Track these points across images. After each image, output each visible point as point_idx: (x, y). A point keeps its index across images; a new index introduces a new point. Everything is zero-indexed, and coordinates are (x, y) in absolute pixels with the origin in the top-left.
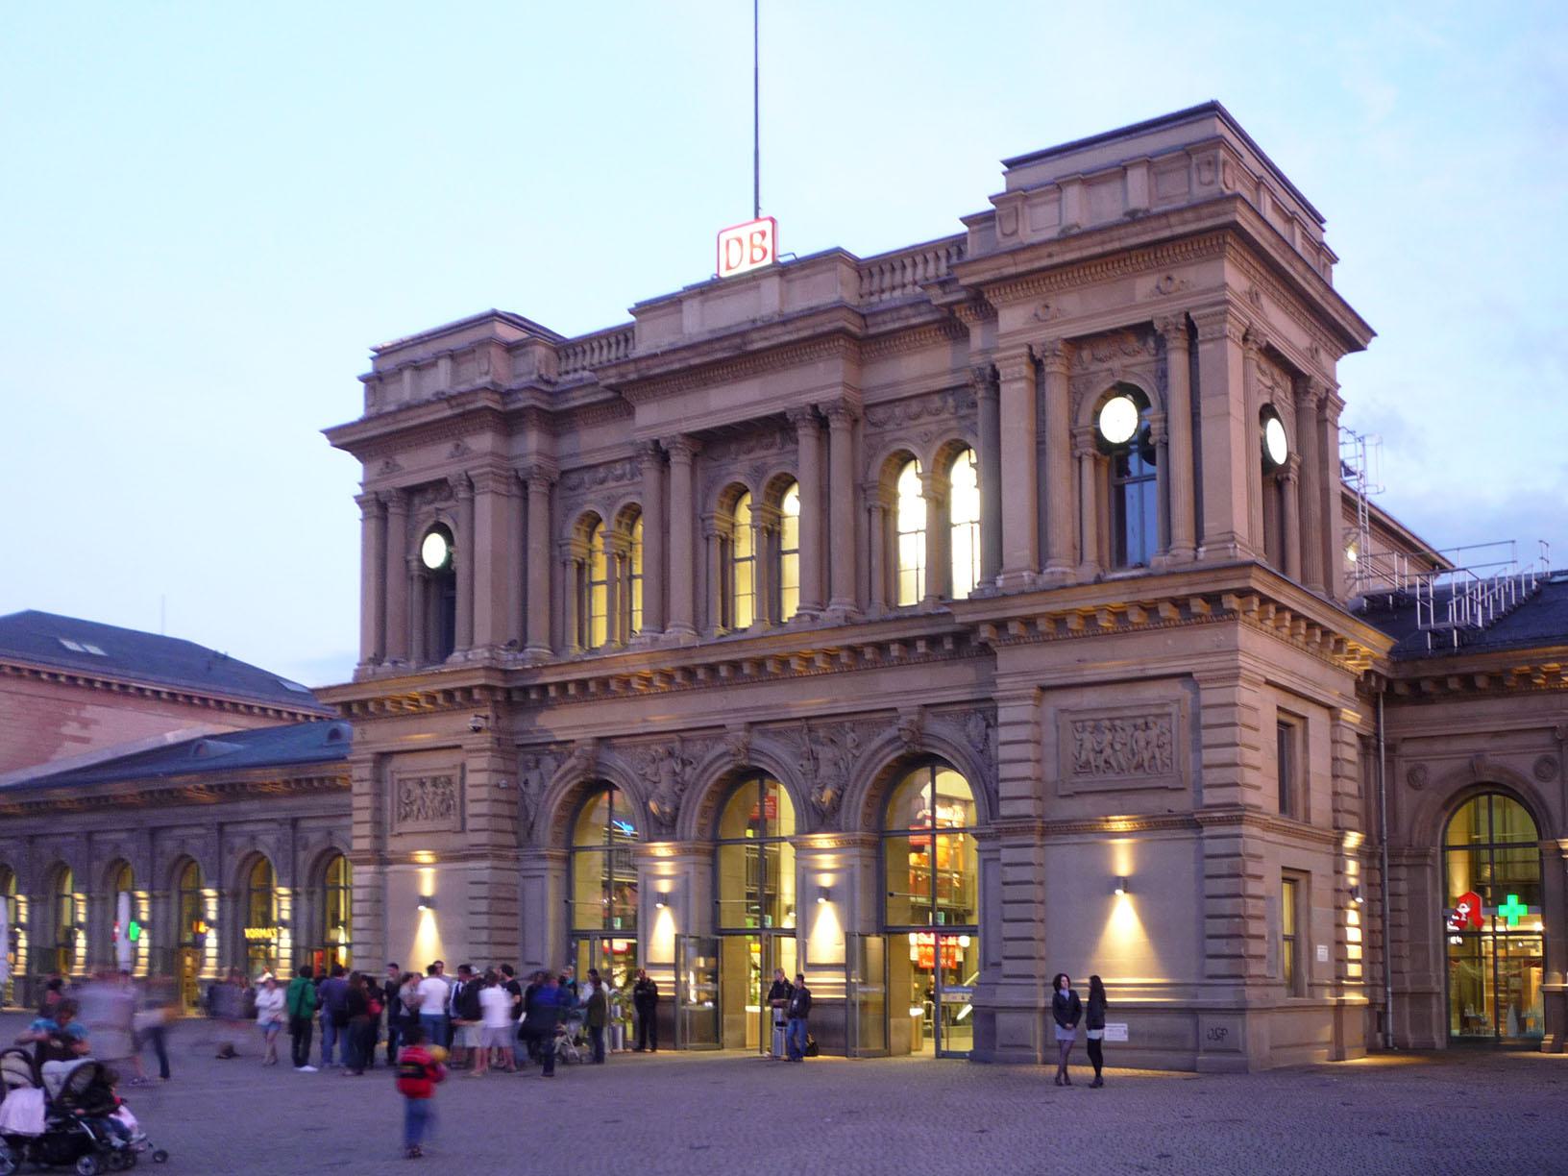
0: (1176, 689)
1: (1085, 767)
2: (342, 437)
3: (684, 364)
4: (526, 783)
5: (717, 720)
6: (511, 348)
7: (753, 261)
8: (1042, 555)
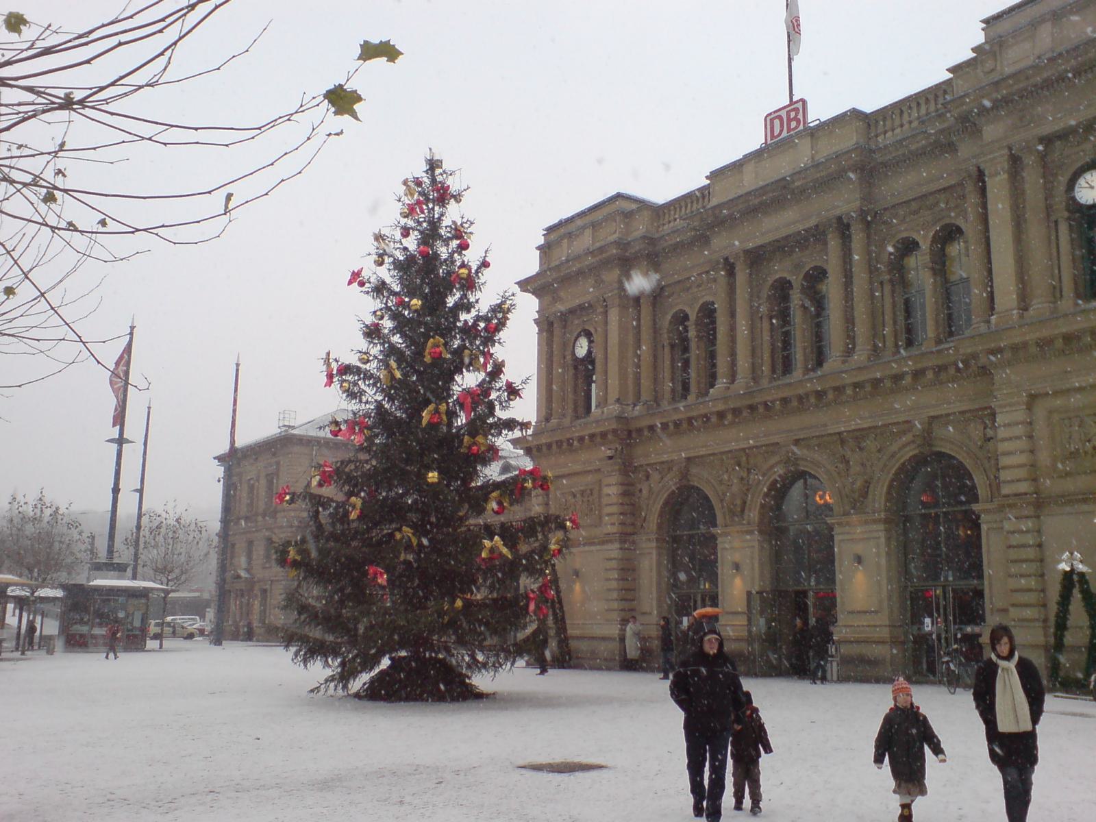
7: (789, 130)
8: (1024, 302)
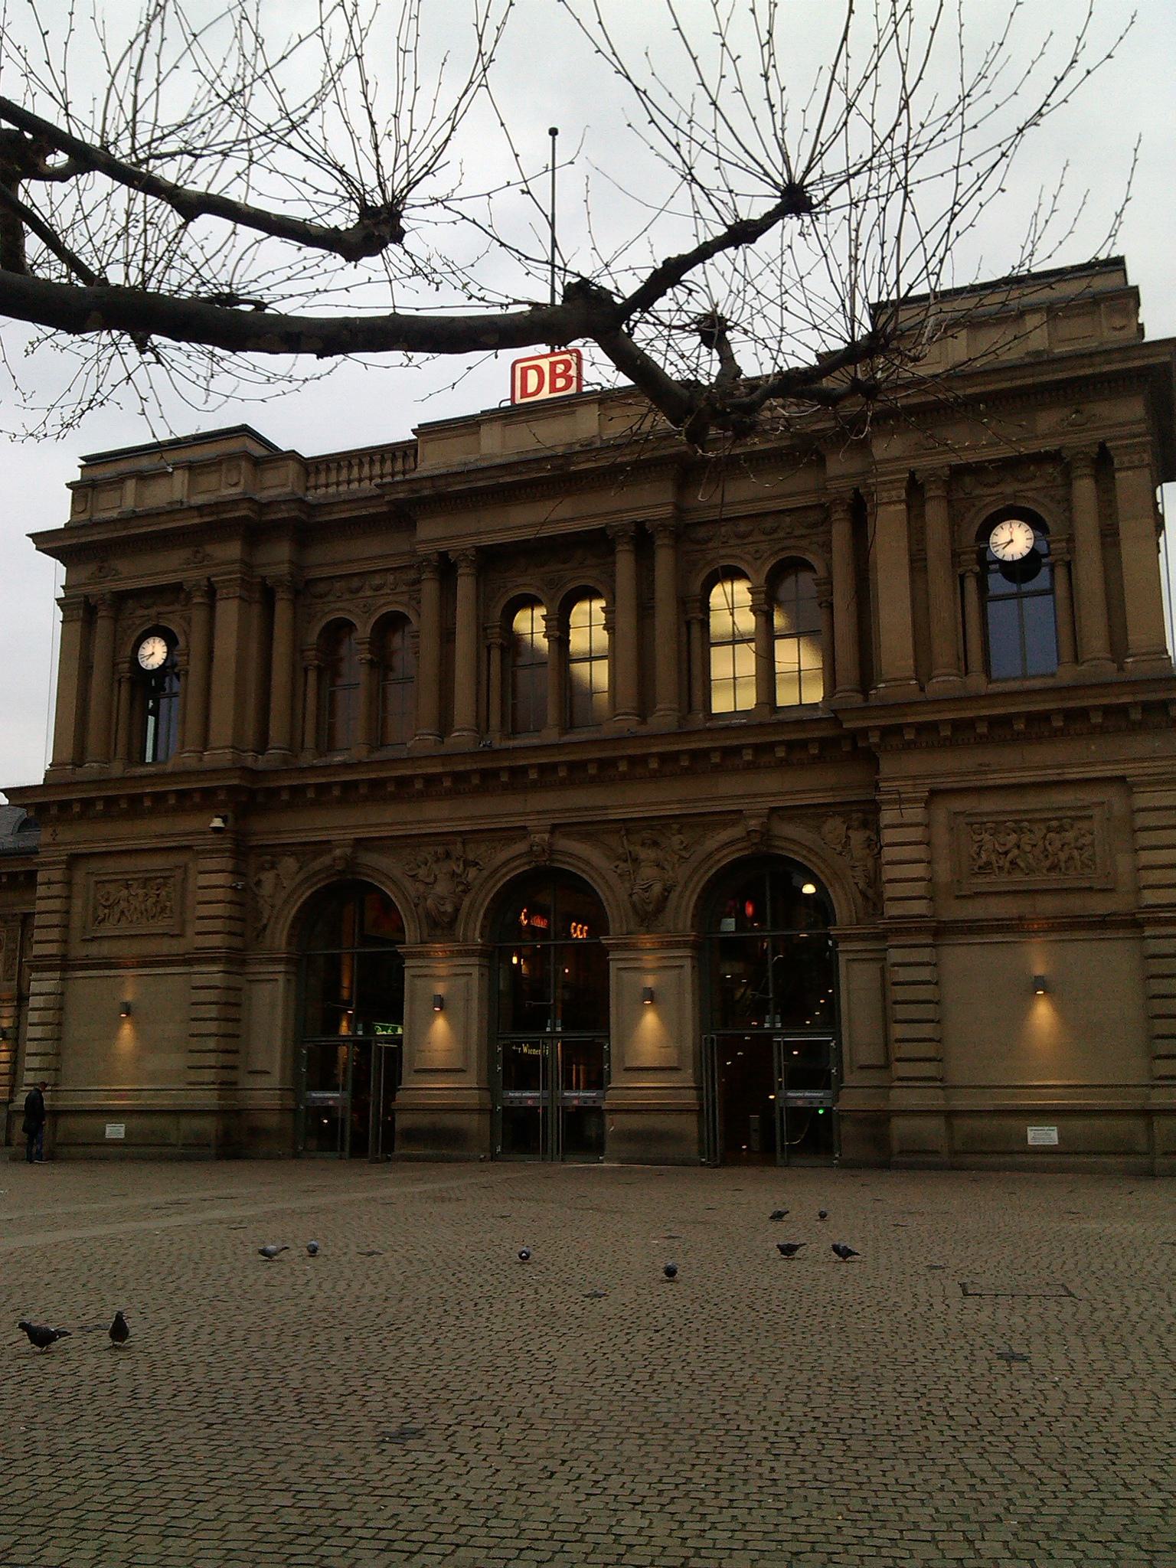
0: (1113, 797)
1: (985, 868)
2: (44, 541)
3: (491, 482)
4: (259, 883)
5: (517, 822)
6: (257, 463)
7: (553, 389)
8: (923, 670)
